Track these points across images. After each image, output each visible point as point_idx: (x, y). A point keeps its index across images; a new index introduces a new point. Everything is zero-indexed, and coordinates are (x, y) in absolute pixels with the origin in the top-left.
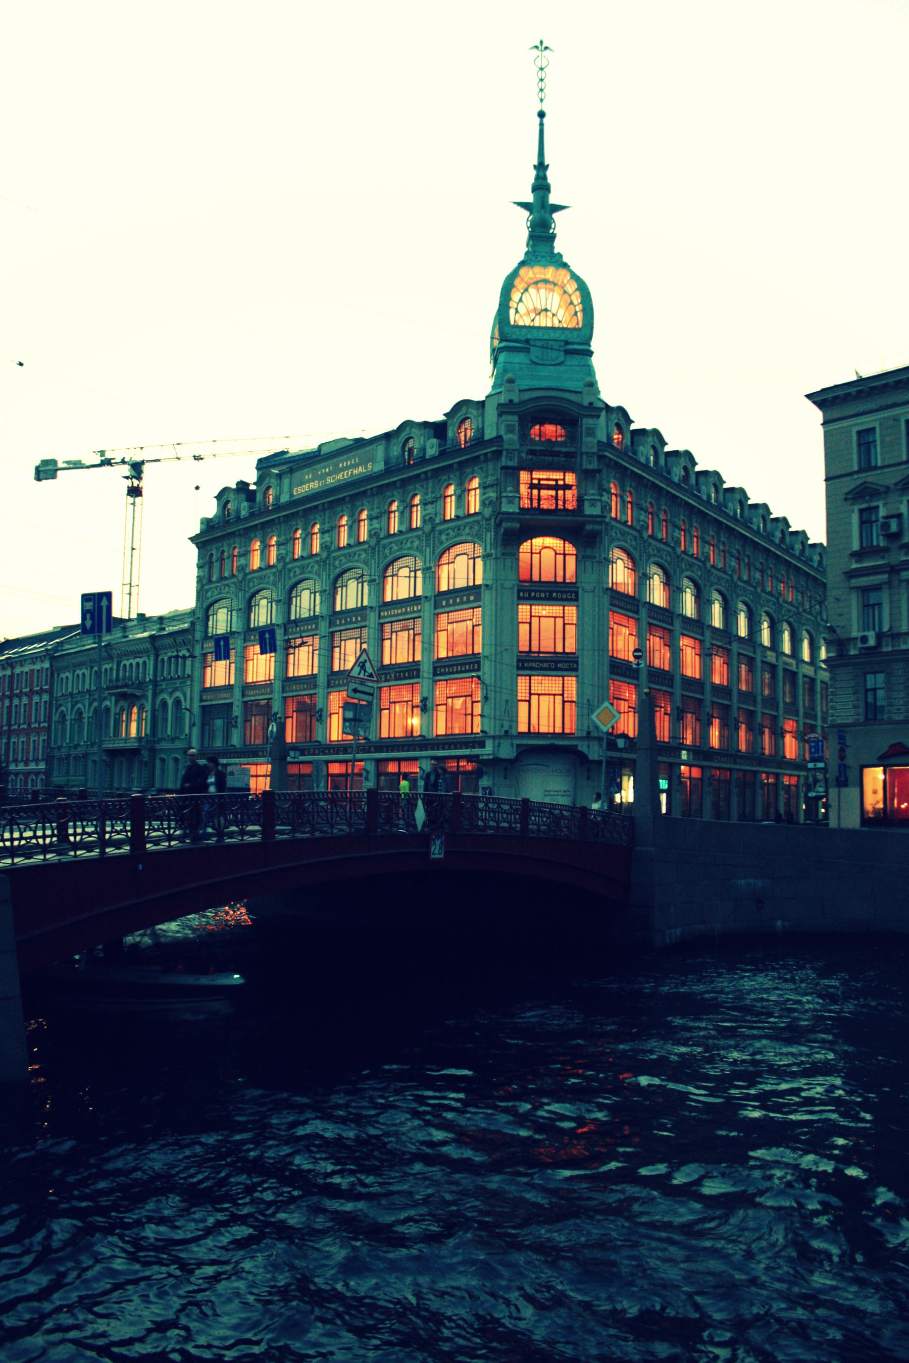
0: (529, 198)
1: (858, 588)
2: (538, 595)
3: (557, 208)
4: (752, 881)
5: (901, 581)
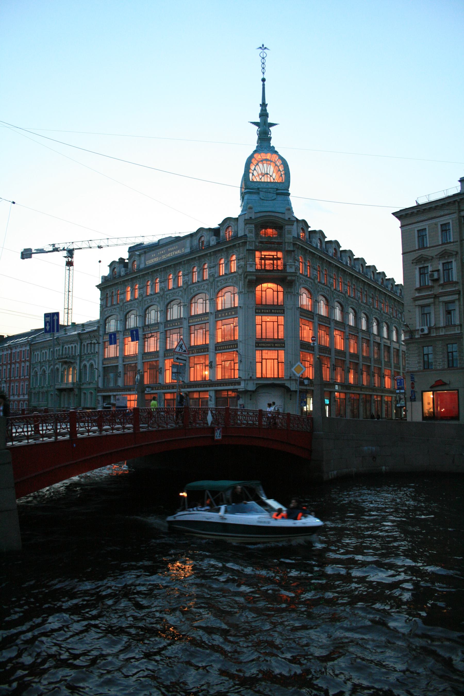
0: (258, 120)
1: (419, 305)
2: (265, 311)
3: (272, 125)
4: (370, 447)
5: (439, 302)
